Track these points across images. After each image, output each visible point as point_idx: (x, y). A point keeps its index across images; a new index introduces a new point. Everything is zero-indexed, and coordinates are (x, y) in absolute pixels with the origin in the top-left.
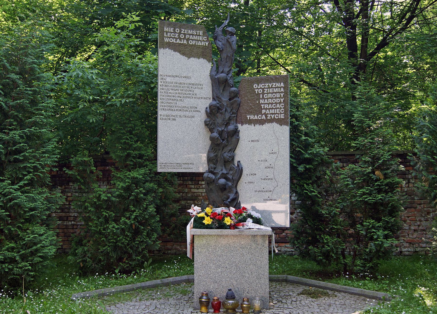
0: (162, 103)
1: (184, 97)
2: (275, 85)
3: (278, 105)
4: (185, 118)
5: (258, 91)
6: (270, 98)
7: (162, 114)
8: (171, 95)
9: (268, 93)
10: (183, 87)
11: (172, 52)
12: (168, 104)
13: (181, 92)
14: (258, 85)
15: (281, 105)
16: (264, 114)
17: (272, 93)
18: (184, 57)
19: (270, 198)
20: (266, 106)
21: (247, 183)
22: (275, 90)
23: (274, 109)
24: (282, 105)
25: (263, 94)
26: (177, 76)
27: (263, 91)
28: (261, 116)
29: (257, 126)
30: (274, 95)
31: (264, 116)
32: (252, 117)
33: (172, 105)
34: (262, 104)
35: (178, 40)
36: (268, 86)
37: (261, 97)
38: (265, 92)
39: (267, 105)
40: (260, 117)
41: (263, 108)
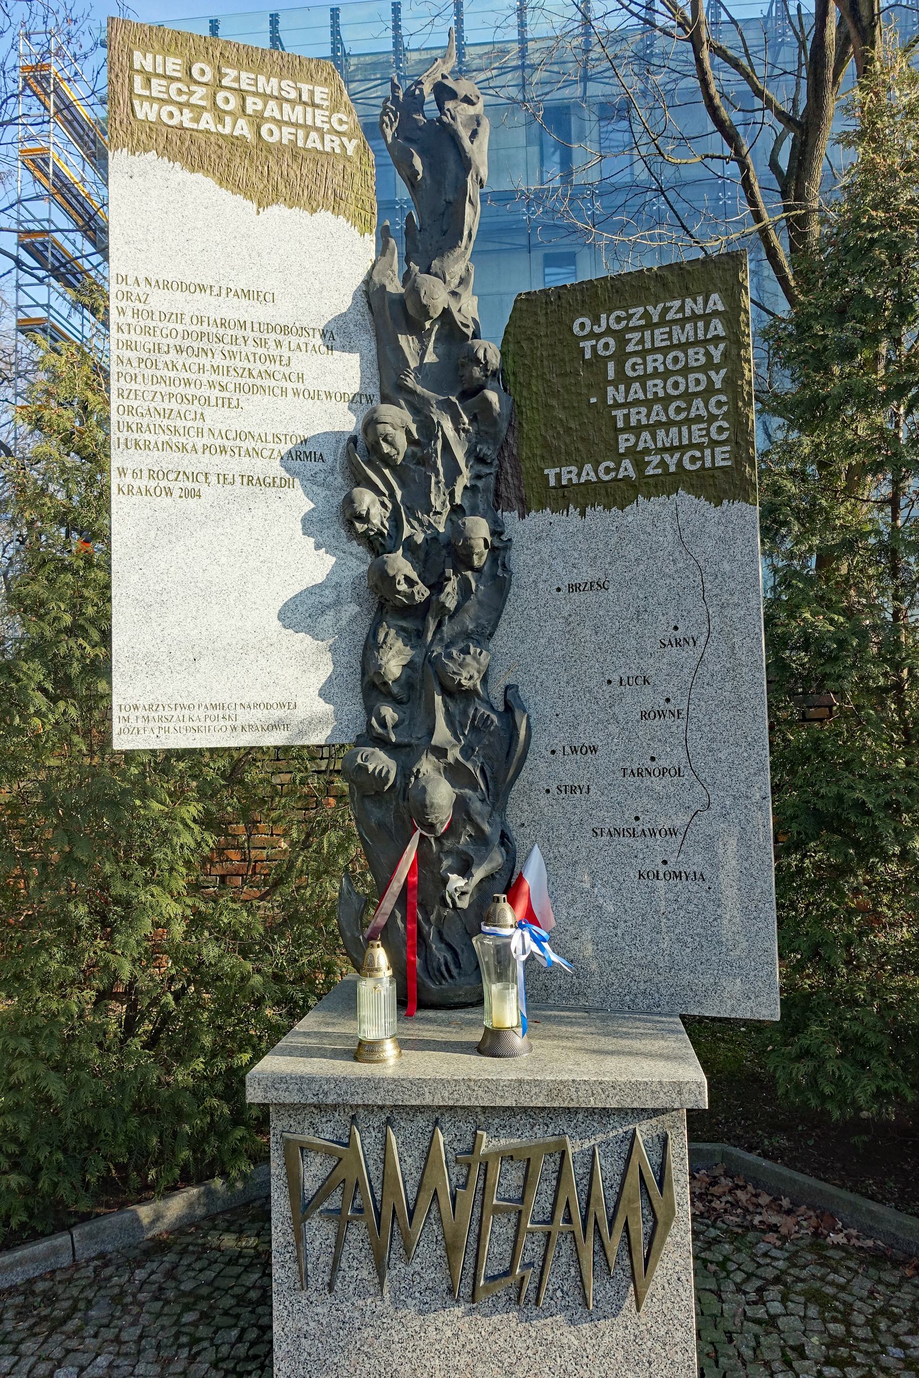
0: (130, 411)
1: (239, 388)
2: (682, 309)
3: (698, 402)
4: (246, 489)
5: (594, 348)
6: (656, 374)
7: (130, 466)
8: (172, 374)
9: (643, 354)
10: (234, 340)
11: (179, 174)
12: (158, 420)
13: (226, 363)
14: (596, 321)
15: (713, 401)
16: (631, 452)
17: (665, 351)
18: (239, 197)
19: (671, 867)
20: (638, 416)
21: (554, 790)
22: (680, 336)
23: (679, 424)
24: (719, 404)
25: (621, 357)
26: (202, 288)
27: (622, 342)
28: (612, 465)
29: (598, 516)
30: (676, 360)
31: (626, 463)
32: (569, 474)
33: (180, 423)
34: (617, 406)
35: (206, 116)
36: (646, 315)
37: (611, 374)
38: (630, 348)
39: (644, 410)
40: (608, 470)
41: (620, 424)
